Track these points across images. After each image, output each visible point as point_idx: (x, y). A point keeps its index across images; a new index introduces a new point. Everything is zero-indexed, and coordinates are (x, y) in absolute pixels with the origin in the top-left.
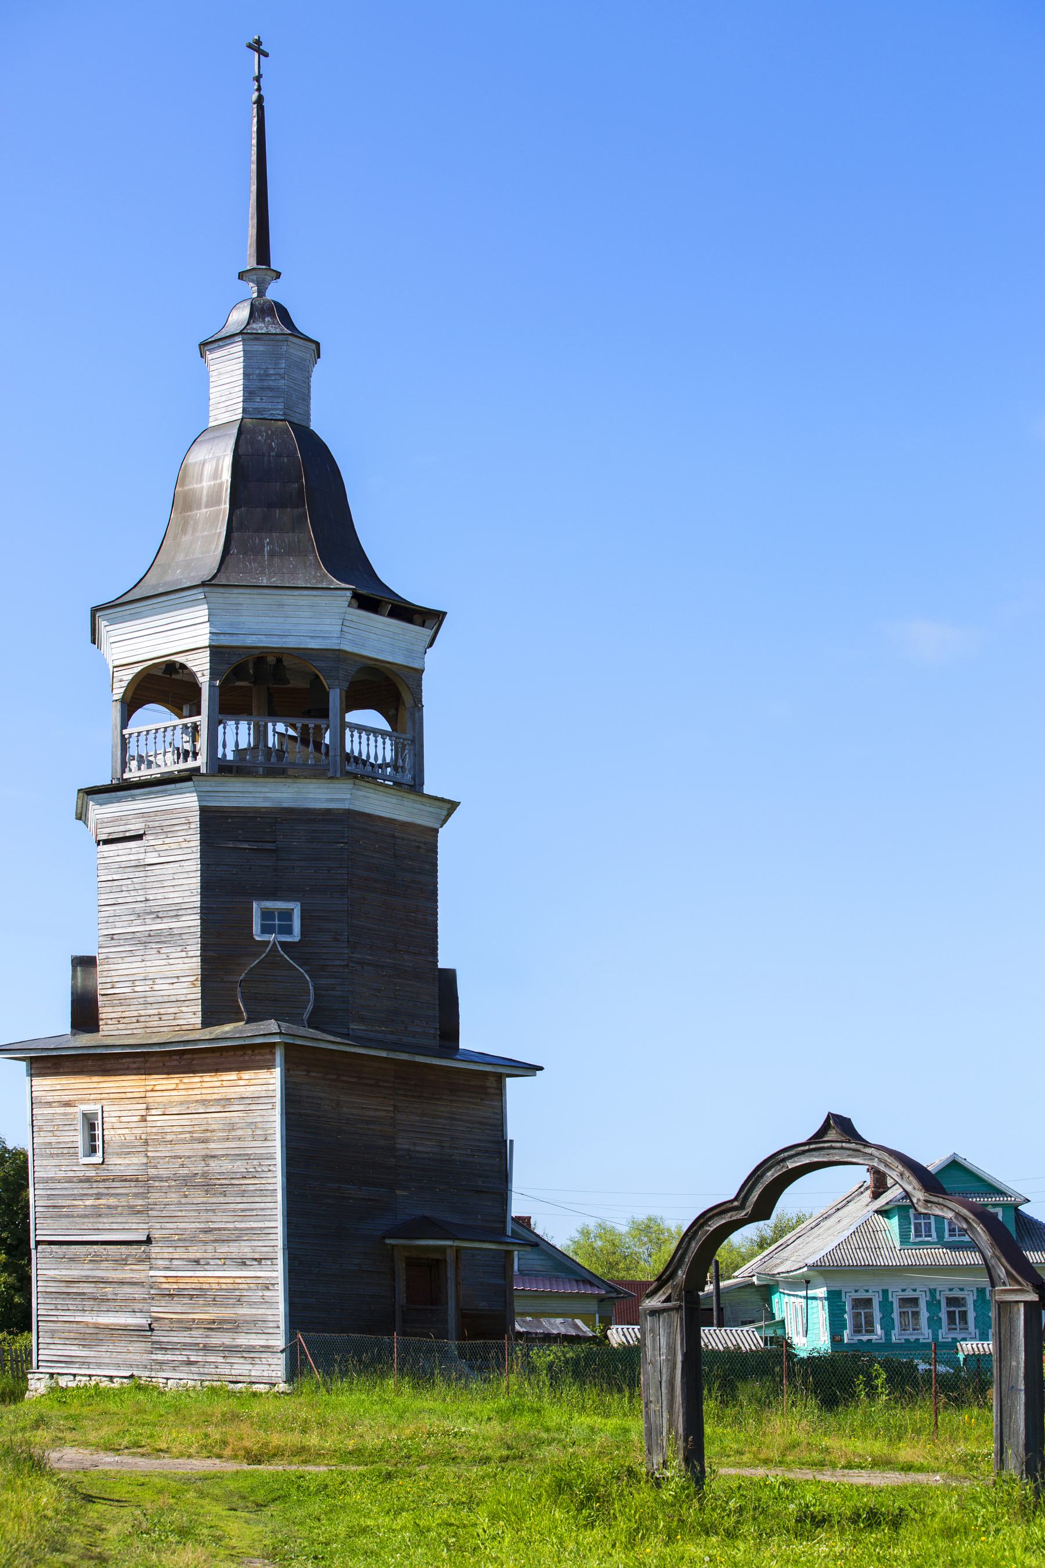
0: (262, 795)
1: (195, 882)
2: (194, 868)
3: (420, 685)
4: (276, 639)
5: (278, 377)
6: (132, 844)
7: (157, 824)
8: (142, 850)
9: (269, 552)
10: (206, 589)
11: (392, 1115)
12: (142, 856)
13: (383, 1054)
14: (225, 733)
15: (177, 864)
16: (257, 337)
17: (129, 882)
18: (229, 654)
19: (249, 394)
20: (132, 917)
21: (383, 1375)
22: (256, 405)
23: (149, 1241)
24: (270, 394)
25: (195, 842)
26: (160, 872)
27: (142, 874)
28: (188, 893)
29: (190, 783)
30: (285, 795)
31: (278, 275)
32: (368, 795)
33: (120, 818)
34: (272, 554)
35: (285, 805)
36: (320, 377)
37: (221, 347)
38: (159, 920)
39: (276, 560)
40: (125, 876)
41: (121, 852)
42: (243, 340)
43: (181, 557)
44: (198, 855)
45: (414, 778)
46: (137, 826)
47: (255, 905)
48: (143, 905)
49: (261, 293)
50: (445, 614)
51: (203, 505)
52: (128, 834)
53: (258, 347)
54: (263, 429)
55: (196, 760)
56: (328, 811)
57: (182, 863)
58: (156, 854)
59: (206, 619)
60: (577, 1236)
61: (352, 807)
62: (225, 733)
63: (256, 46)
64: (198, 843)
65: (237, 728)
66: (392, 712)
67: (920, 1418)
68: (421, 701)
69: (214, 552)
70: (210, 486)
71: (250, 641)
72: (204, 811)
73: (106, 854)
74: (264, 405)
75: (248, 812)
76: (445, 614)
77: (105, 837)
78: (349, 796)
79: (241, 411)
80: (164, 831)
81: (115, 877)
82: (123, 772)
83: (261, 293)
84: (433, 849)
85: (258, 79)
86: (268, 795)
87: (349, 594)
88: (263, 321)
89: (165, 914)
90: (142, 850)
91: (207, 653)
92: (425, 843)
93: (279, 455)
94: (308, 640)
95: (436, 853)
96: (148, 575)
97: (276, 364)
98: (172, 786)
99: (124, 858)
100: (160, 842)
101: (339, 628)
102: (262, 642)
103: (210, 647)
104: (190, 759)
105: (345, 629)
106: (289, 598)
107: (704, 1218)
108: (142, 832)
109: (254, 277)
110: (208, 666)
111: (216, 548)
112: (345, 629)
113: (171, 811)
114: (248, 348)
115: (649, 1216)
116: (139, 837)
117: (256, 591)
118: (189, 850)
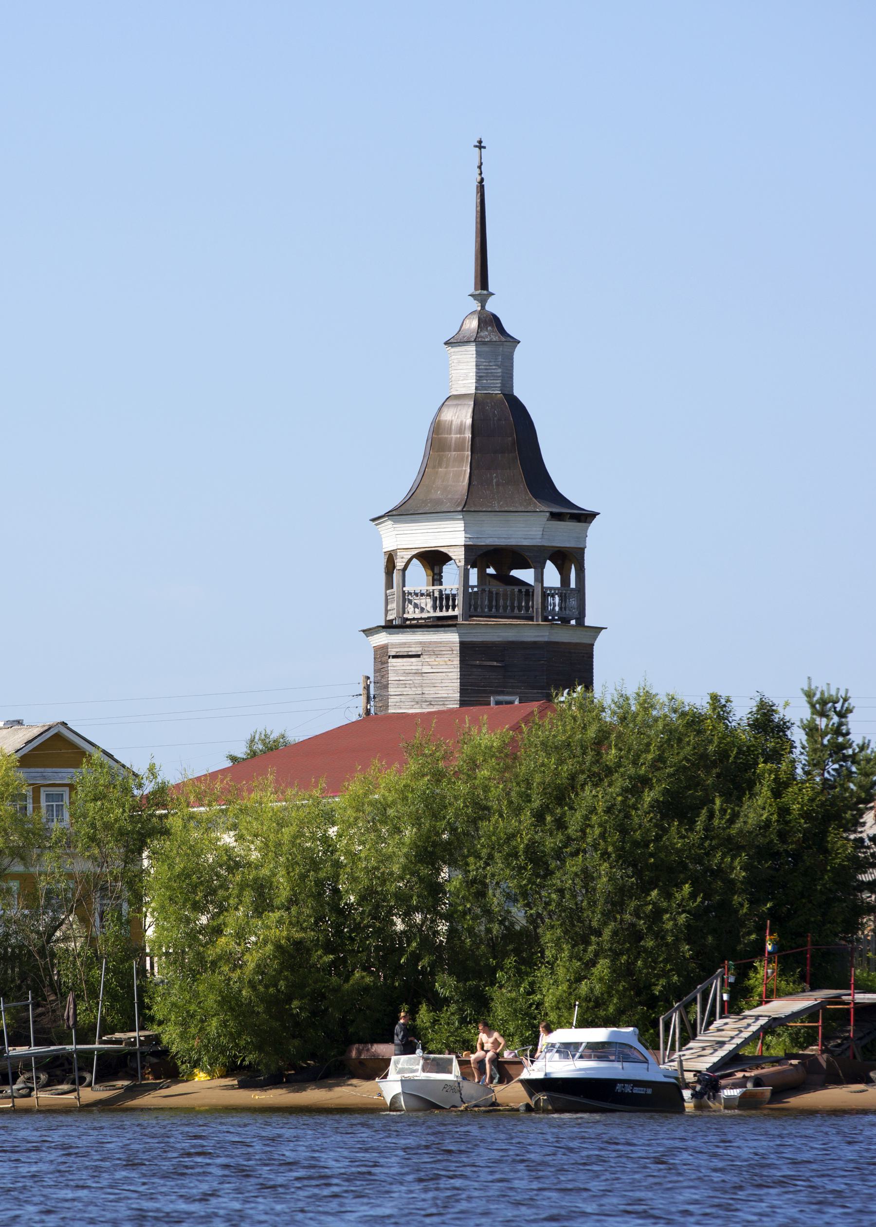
1: (457, 684)
2: (456, 677)
3: (583, 557)
4: (503, 540)
6: (413, 660)
7: (430, 649)
8: (421, 663)
9: (496, 483)
10: (464, 513)
12: (420, 667)
15: (444, 674)
16: (484, 343)
17: (411, 682)
19: (479, 378)
20: (413, 704)
25: (457, 662)
26: (431, 678)
27: (419, 678)
28: (451, 692)
29: (455, 628)
30: (510, 634)
33: (405, 644)
34: (498, 484)
35: (510, 639)
36: (519, 354)
37: (459, 346)
38: (432, 706)
39: (501, 488)
40: (409, 678)
41: (405, 664)
42: (476, 345)
43: (439, 482)
44: (459, 670)
45: (580, 613)
46: (417, 649)
47: (492, 698)
48: (420, 696)
49: (483, 307)
50: (519, 342)
51: (452, 449)
52: (410, 653)
53: (485, 349)
54: (488, 401)
55: (454, 610)
56: (535, 643)
57: (448, 674)
58: (430, 667)
59: (463, 529)
63: (480, 146)
64: (458, 663)
66: (559, 562)
67: (617, 707)
68: (584, 567)
69: (463, 482)
70: (457, 438)
72: (462, 644)
73: (395, 664)
76: (519, 342)
77: (394, 654)
79: (474, 388)
80: (436, 654)
81: (401, 678)
82: (404, 612)
83: (483, 307)
84: (591, 656)
85: (480, 167)
87: (548, 514)
88: (487, 330)
89: (436, 703)
90: (421, 663)
91: (463, 548)
92: (587, 653)
93: (499, 420)
96: (417, 491)
97: (496, 359)
98: (443, 629)
99: (408, 668)
100: (433, 660)
101: (541, 533)
102: (494, 542)
103: (465, 546)
104: (450, 610)
105: (545, 533)
106: (511, 517)
107: (202, 1223)
108: (420, 653)
109: (479, 298)
110: (463, 557)
111: (463, 481)
112: (545, 533)
113: (440, 643)
114: (479, 349)
116: (418, 656)
117: (493, 513)
118: (452, 666)
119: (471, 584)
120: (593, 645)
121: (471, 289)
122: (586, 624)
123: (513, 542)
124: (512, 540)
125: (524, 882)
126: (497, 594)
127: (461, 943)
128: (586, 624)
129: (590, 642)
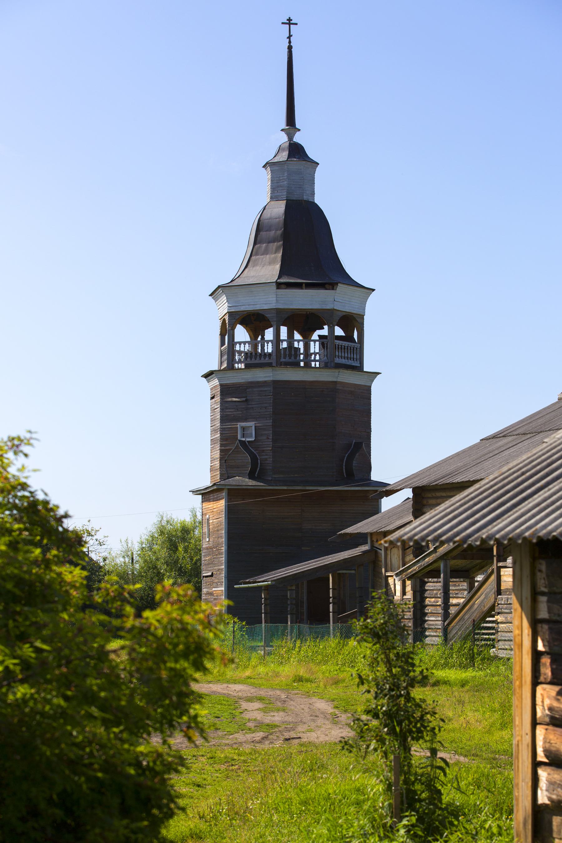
0: (241, 377)
4: (252, 306)
5: (284, 180)
11: (300, 514)
13: (285, 488)
14: (267, 348)
18: (235, 315)
21: (322, 635)
22: (276, 194)
23: (212, 576)
24: (281, 188)
30: (249, 376)
31: (299, 130)
32: (284, 372)
35: (250, 380)
50: (318, 164)
53: (276, 168)
60: (61, 512)
61: (274, 379)
62: (267, 348)
65: (315, 345)
71: (242, 308)
72: (221, 385)
74: (278, 194)
75: (237, 385)
76: (318, 164)
78: (272, 375)
86: (243, 377)
94: (264, 305)
95: (370, 400)
101: (275, 299)
104: (253, 359)
112: (278, 299)
115: (50, 501)
119: (282, 338)
120: (370, 387)
121: (284, 125)
122: (365, 370)
123: (258, 307)
124: (257, 306)
125: (38, 538)
126: (347, 347)
127: (386, 762)
128: (365, 370)
129: (369, 385)
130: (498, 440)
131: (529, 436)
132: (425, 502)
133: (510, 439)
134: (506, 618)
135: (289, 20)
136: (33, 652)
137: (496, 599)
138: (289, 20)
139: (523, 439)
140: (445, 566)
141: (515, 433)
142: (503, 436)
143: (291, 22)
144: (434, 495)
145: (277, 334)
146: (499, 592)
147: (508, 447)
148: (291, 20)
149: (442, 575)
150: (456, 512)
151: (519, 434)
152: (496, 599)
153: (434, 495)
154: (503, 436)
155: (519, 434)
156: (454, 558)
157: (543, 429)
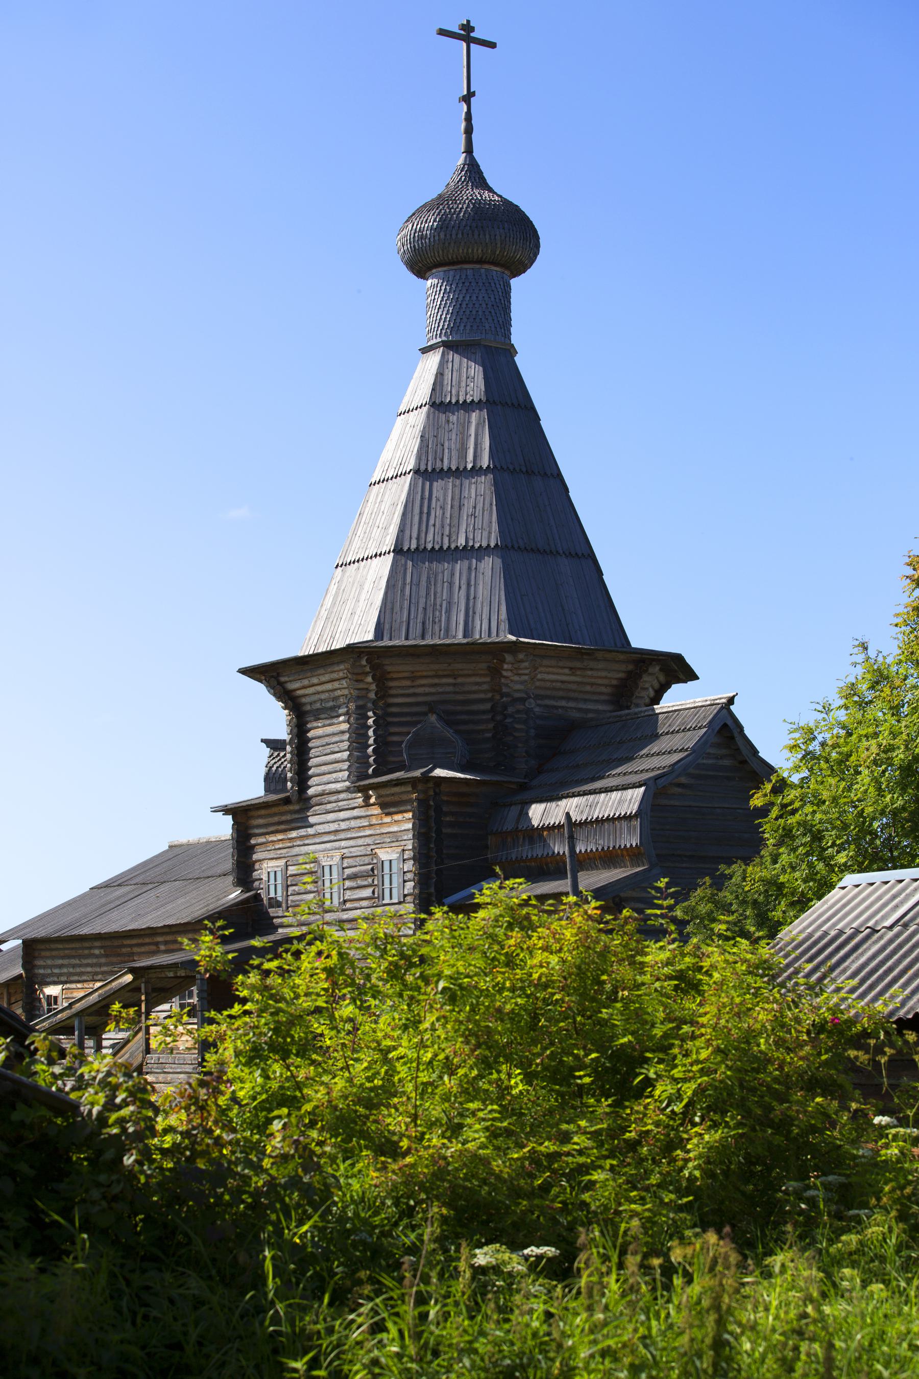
130: (112, 889)
131: (151, 886)
132: (36, 954)
133: (128, 888)
134: (157, 1078)
135: (468, 28)
136: (716, 1132)
137: (144, 1058)
138: (468, 28)
139: (145, 889)
140: (80, 1023)
141: (132, 882)
142: (119, 885)
143: (472, 35)
144: (48, 946)
145: (506, 670)
146: (148, 1050)
147: (130, 897)
148: (472, 29)
149: (76, 1033)
150: (896, 957)
151: (137, 884)
152: (144, 1058)
153: (48, 946)
154: (119, 885)
155: (137, 884)
156: (90, 1015)
157: (166, 879)
